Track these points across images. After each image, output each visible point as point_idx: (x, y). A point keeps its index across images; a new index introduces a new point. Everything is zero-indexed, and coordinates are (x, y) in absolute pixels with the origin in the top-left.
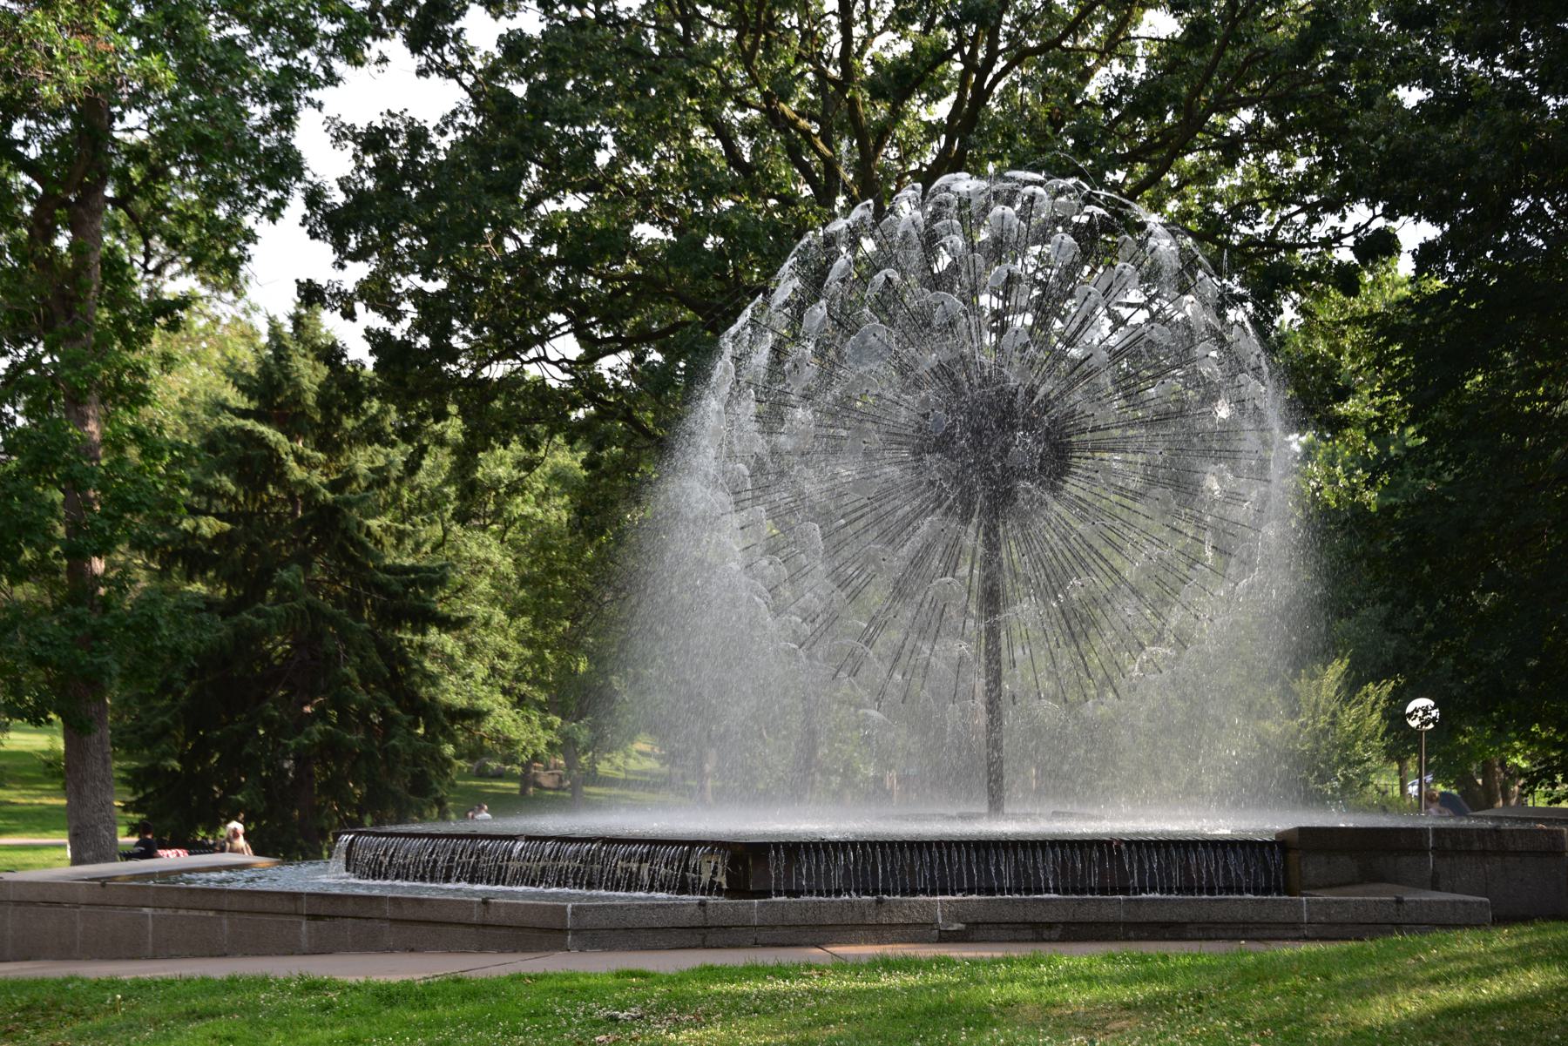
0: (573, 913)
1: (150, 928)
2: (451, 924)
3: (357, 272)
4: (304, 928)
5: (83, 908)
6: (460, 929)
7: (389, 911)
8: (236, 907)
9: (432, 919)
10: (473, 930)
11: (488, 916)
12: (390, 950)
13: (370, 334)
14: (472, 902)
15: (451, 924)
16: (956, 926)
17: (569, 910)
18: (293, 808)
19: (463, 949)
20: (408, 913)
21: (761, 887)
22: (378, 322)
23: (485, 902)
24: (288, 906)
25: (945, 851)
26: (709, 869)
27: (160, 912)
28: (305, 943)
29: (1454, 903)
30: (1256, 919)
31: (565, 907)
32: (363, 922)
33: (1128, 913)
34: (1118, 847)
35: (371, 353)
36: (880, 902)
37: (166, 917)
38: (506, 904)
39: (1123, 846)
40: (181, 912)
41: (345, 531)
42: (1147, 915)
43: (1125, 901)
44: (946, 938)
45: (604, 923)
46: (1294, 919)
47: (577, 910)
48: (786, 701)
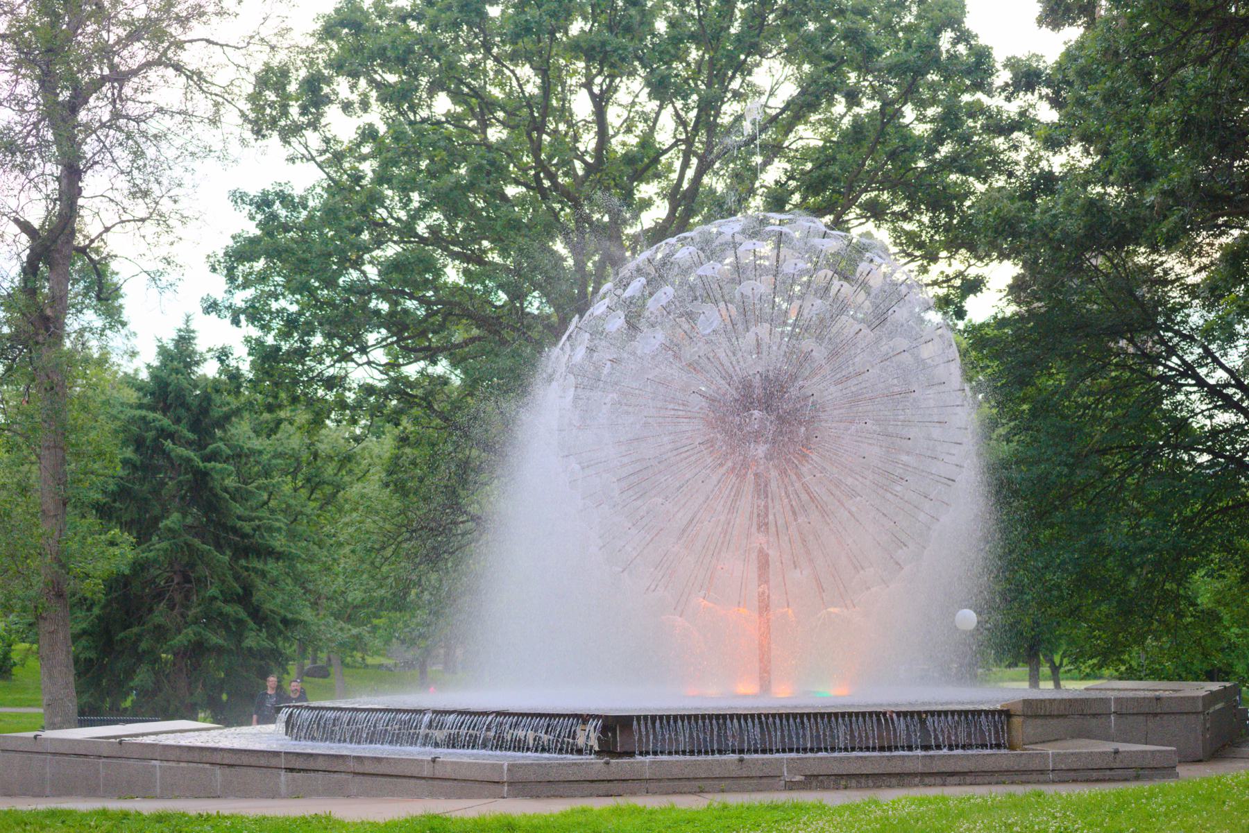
0: (508, 770)
1: (158, 774)
2: (405, 777)
3: (241, 298)
4: (283, 778)
5: (104, 760)
6: (413, 781)
7: (352, 766)
8: (226, 762)
9: (389, 773)
10: (423, 781)
11: (436, 772)
12: (356, 796)
13: (248, 340)
14: (422, 760)
15: (405, 777)
16: (798, 778)
17: (505, 768)
18: (221, 692)
19: (448, 796)
20: (369, 768)
21: (627, 748)
22: (254, 332)
23: (434, 760)
24: (185, 756)
25: (742, 721)
26: (588, 736)
27: (165, 764)
28: (283, 789)
29: (1153, 752)
30: (1016, 768)
31: (502, 765)
32: (332, 775)
33: (924, 765)
34: (891, 716)
35: (249, 354)
36: (741, 760)
37: (170, 768)
38: (452, 762)
39: (894, 715)
40: (182, 764)
41: (211, 489)
42: (938, 767)
43: (923, 757)
44: (791, 786)
45: (532, 778)
46: (1043, 767)
47: (512, 768)
48: (32, 551)
